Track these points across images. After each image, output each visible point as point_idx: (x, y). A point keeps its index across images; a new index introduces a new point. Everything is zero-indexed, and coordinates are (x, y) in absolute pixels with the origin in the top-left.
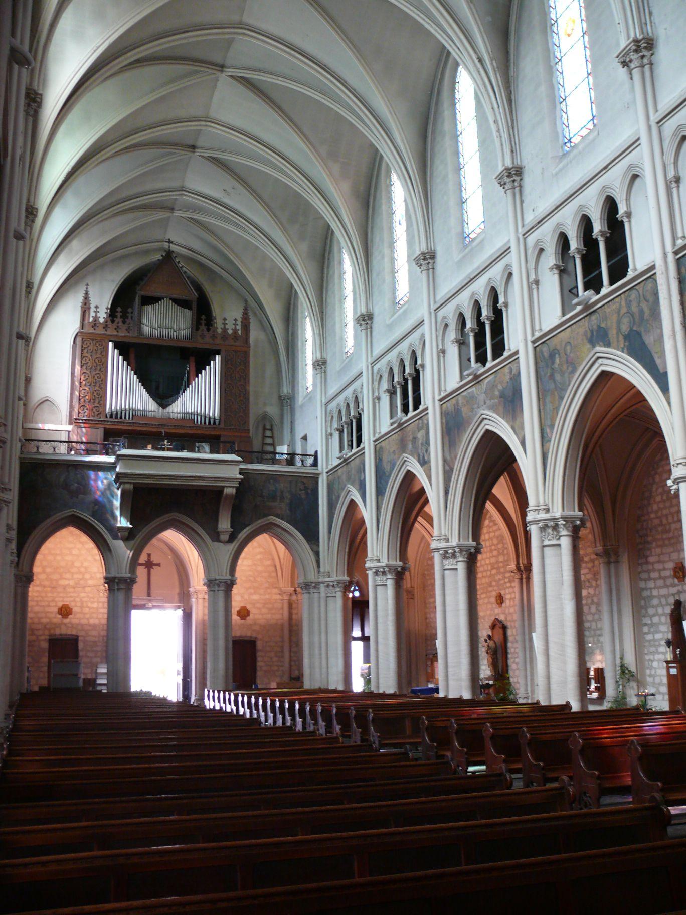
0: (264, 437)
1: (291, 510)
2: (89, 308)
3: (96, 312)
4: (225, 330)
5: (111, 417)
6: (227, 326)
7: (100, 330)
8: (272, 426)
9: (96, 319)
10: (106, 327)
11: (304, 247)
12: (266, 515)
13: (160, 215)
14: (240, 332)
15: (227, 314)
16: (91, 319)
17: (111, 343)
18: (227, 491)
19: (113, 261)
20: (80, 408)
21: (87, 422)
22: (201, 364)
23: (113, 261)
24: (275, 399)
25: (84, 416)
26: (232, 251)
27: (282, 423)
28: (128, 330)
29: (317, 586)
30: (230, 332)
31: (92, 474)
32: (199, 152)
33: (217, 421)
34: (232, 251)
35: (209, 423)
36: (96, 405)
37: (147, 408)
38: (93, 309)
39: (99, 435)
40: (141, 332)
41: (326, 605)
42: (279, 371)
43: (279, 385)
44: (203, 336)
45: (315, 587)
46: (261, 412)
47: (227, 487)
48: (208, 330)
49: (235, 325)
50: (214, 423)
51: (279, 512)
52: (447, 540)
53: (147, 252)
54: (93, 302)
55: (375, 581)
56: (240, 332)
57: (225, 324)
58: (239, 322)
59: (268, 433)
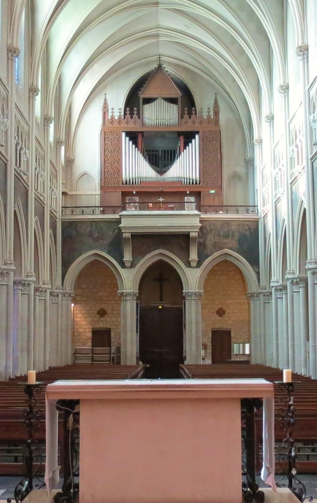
1: (239, 245)
2: (108, 110)
3: (113, 112)
5: (126, 183)
9: (112, 117)
10: (119, 122)
12: (222, 248)
13: (153, 40)
14: (212, 117)
15: (204, 103)
16: (110, 118)
19: (124, 73)
22: (188, 141)
23: (124, 73)
24: (242, 162)
28: (135, 123)
29: (258, 295)
30: (205, 117)
32: (161, 6)
33: (198, 182)
35: (194, 183)
38: (110, 111)
40: (143, 124)
41: (264, 308)
42: (244, 141)
44: (186, 123)
45: (256, 296)
48: (190, 117)
49: (209, 112)
50: (196, 183)
51: (231, 246)
52: (294, 273)
53: (148, 64)
55: (276, 295)
56: (212, 117)
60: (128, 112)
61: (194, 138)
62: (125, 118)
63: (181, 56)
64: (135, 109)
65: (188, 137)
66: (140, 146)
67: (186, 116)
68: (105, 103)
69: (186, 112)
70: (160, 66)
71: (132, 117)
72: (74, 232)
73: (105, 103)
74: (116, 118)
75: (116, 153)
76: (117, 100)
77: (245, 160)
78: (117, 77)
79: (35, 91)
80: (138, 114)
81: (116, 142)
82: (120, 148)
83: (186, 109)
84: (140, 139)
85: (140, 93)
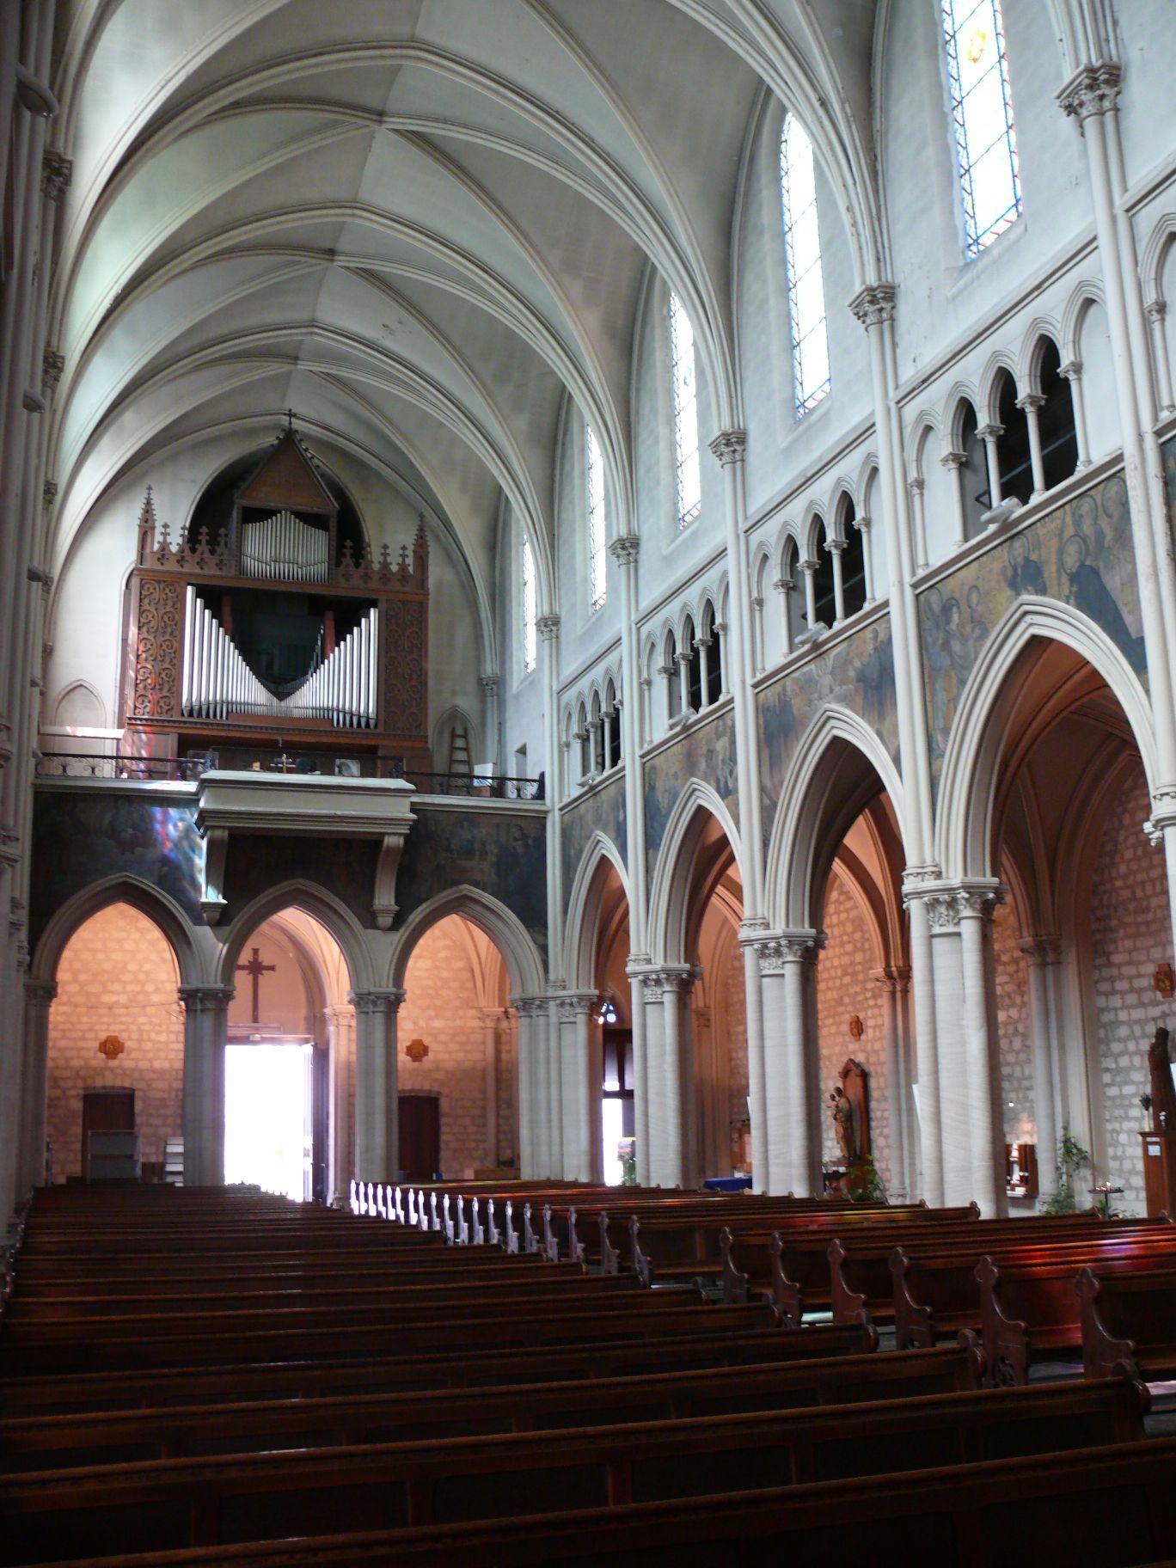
0: (453, 749)
1: (498, 874)
2: (153, 528)
3: (165, 534)
4: (385, 565)
5: (191, 714)
6: (389, 559)
7: (171, 566)
8: (466, 730)
9: (164, 546)
10: (181, 560)
11: (521, 423)
12: (456, 883)
13: (275, 368)
14: (411, 569)
15: (389, 537)
16: (156, 547)
17: (189, 589)
18: (390, 841)
19: (195, 447)
20: (136, 699)
21: (150, 723)
22: (345, 625)
23: (195, 447)
24: (471, 685)
25: (145, 713)
26: (398, 429)
27: (483, 725)
28: (219, 565)
29: (543, 1004)
30: (394, 568)
31: (158, 812)
32: (341, 261)
33: (372, 722)
34: (398, 429)
35: (359, 724)
36: (165, 693)
37: (251, 699)
38: (159, 529)
39: (169, 745)
40: (241, 570)
41: (560, 1037)
42: (478, 637)
43: (479, 659)
44: (347, 576)
45: (539, 1007)
46: (447, 706)
47: (390, 834)
48: (357, 565)
49: (403, 556)
50: (368, 725)
51: (478, 877)
52: (767, 926)
53: (252, 432)
54: (160, 518)
55: (642, 995)
56: (411, 569)
57: (385, 555)
58: (410, 552)
59: (460, 743)
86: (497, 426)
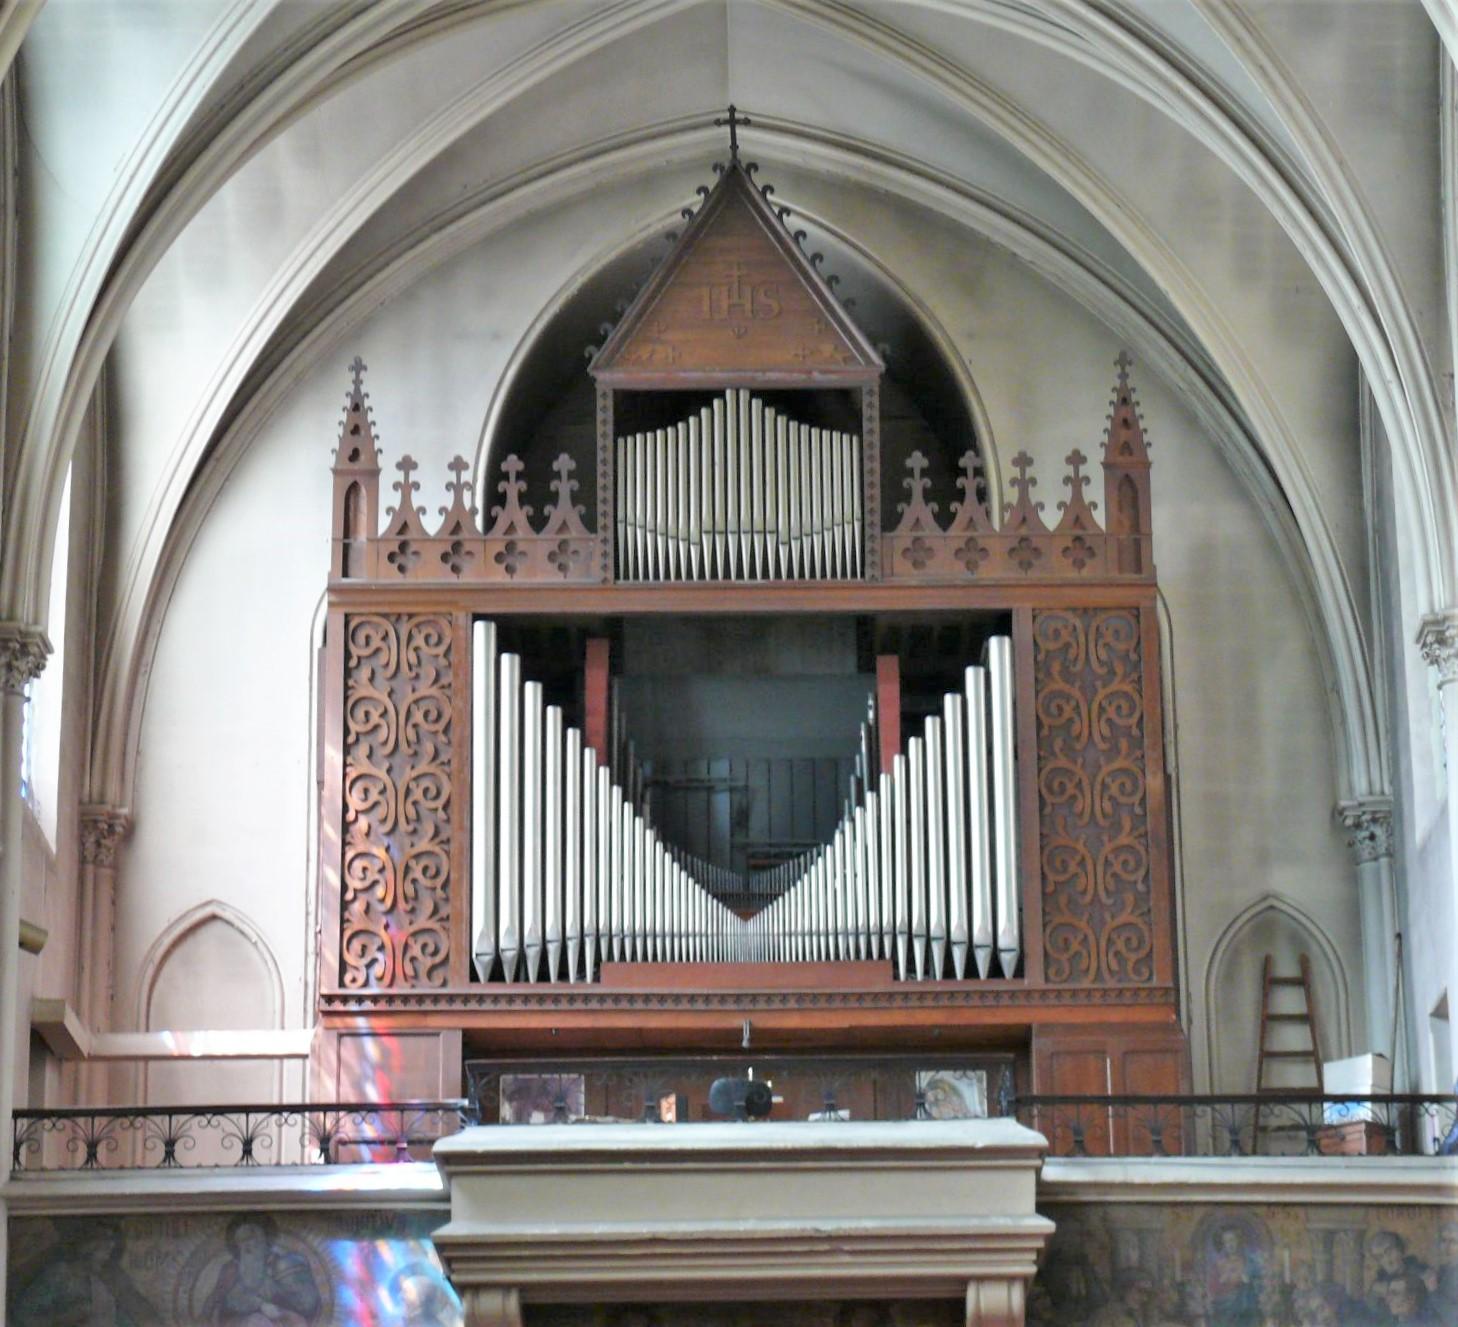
0: (1269, 1020)
2: (374, 473)
3: (407, 488)
4: (1026, 513)
5: (496, 974)
6: (417, 499)
7: (428, 572)
8: (1304, 963)
9: (405, 523)
10: (453, 550)
11: (1325, 64)
14: (1099, 517)
15: (1037, 431)
16: (384, 523)
17: (479, 627)
18: (982, 1300)
20: (345, 944)
21: (387, 1005)
24: (1313, 832)
25: (372, 978)
26: (1040, 127)
27: (1356, 940)
30: (1051, 519)
31: (348, 1254)
34: (1040, 127)
36: (423, 921)
37: (664, 921)
38: (389, 475)
39: (439, 1062)
40: (619, 567)
43: (1332, 761)
44: (918, 553)
46: (1244, 896)
47: (981, 1279)
48: (945, 519)
49: (1076, 482)
50: (996, 970)
53: (648, 182)
54: (390, 440)
56: (1099, 517)
57: (1024, 484)
58: (1094, 469)
59: (1289, 1001)
60: (513, 489)
61: (980, 658)
62: (490, 522)
63: (878, 122)
64: (564, 463)
65: (930, 659)
66: (596, 721)
67: (918, 510)
68: (357, 427)
69: (917, 485)
70: (734, 187)
71: (538, 523)
72: (101, 1293)
73: (357, 427)
74: (432, 524)
75: (423, 766)
76: (440, 420)
77: (1337, 813)
78: (443, 272)
79: (24, 650)
80: (585, 497)
81: (425, 688)
82: (455, 730)
83: (917, 461)
84: (596, 679)
85: (598, 356)
86: (1247, 70)
